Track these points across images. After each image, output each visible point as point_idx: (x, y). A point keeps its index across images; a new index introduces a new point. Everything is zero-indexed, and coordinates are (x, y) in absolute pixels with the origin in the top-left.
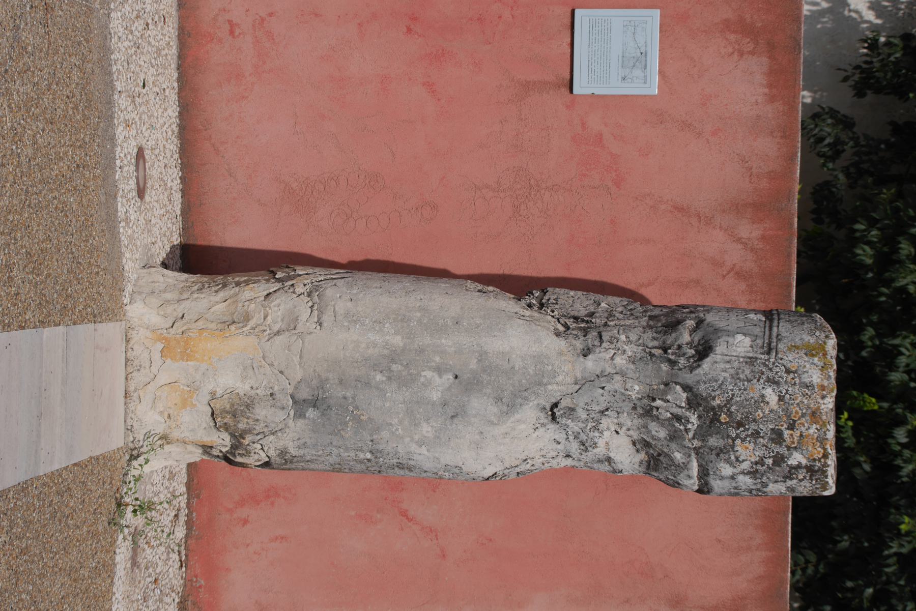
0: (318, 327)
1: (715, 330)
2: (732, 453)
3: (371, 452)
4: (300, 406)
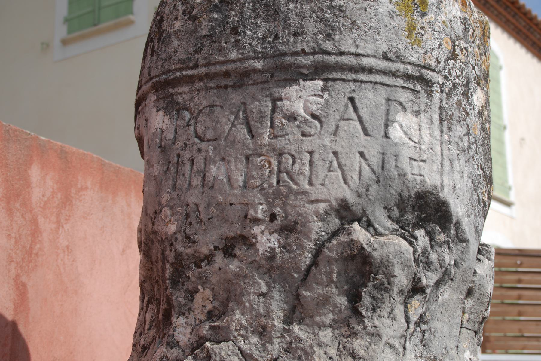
1: (378, 181)
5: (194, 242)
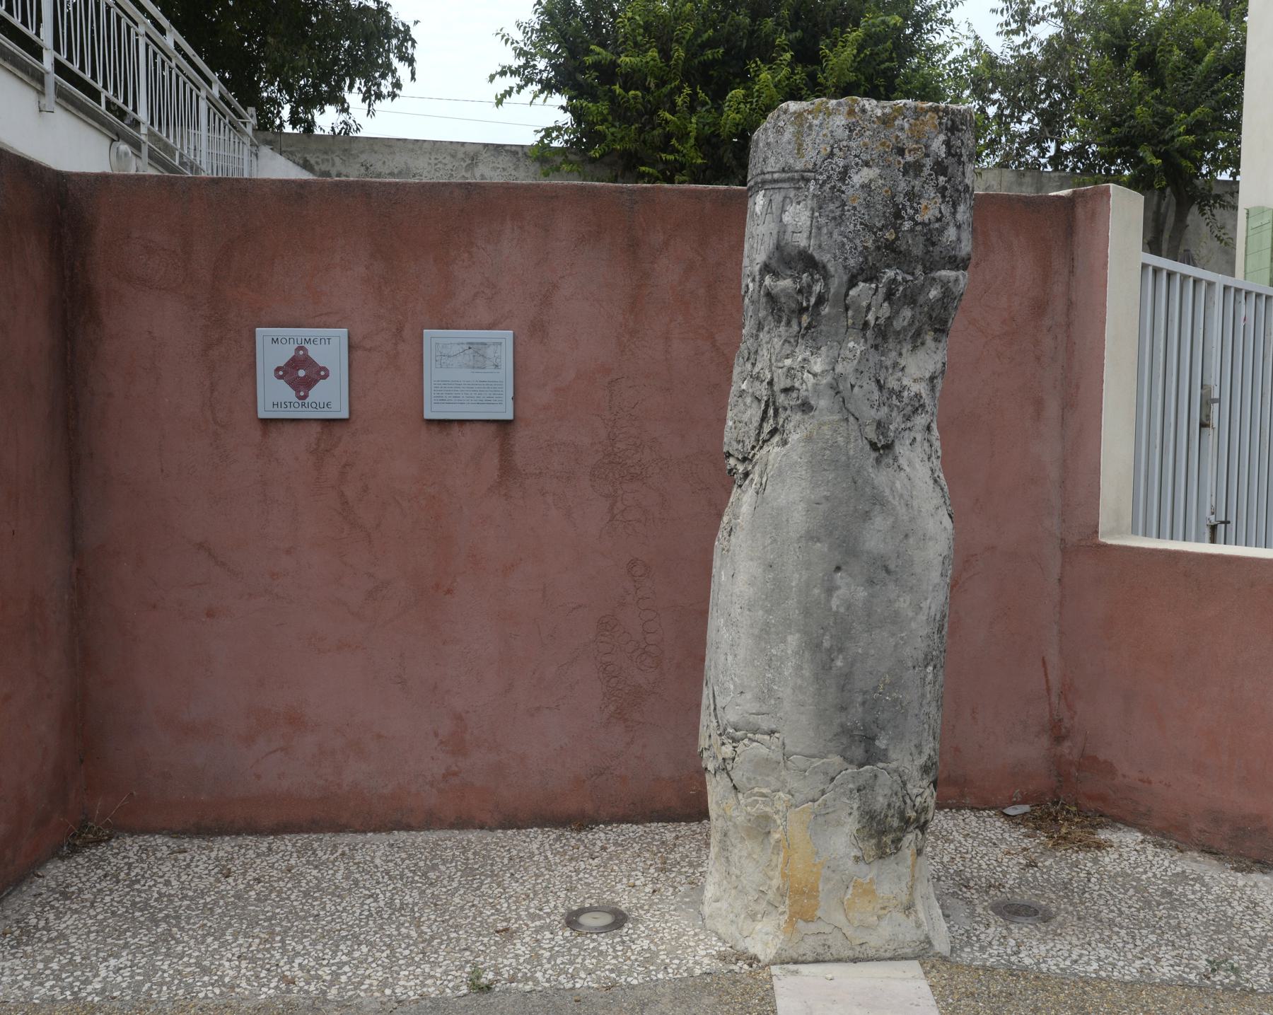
0: (777, 735)
1: (777, 249)
2: (931, 226)
3: (926, 667)
4: (872, 756)
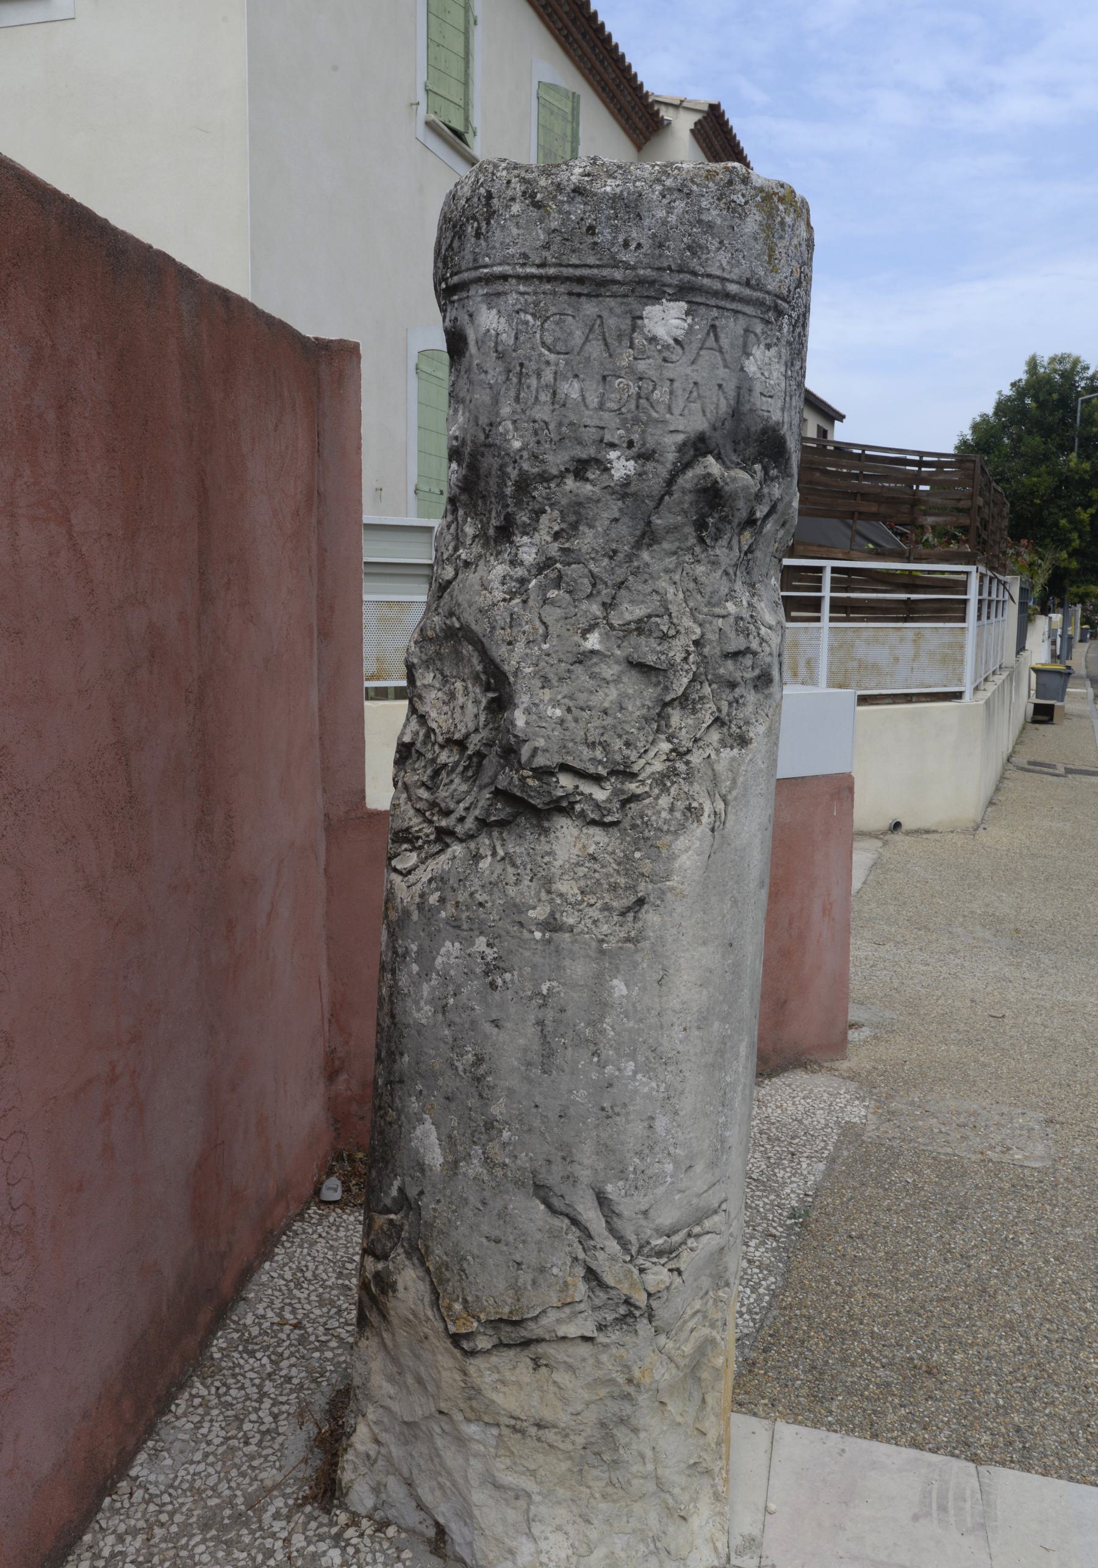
1: (733, 416)
5: (543, 461)
